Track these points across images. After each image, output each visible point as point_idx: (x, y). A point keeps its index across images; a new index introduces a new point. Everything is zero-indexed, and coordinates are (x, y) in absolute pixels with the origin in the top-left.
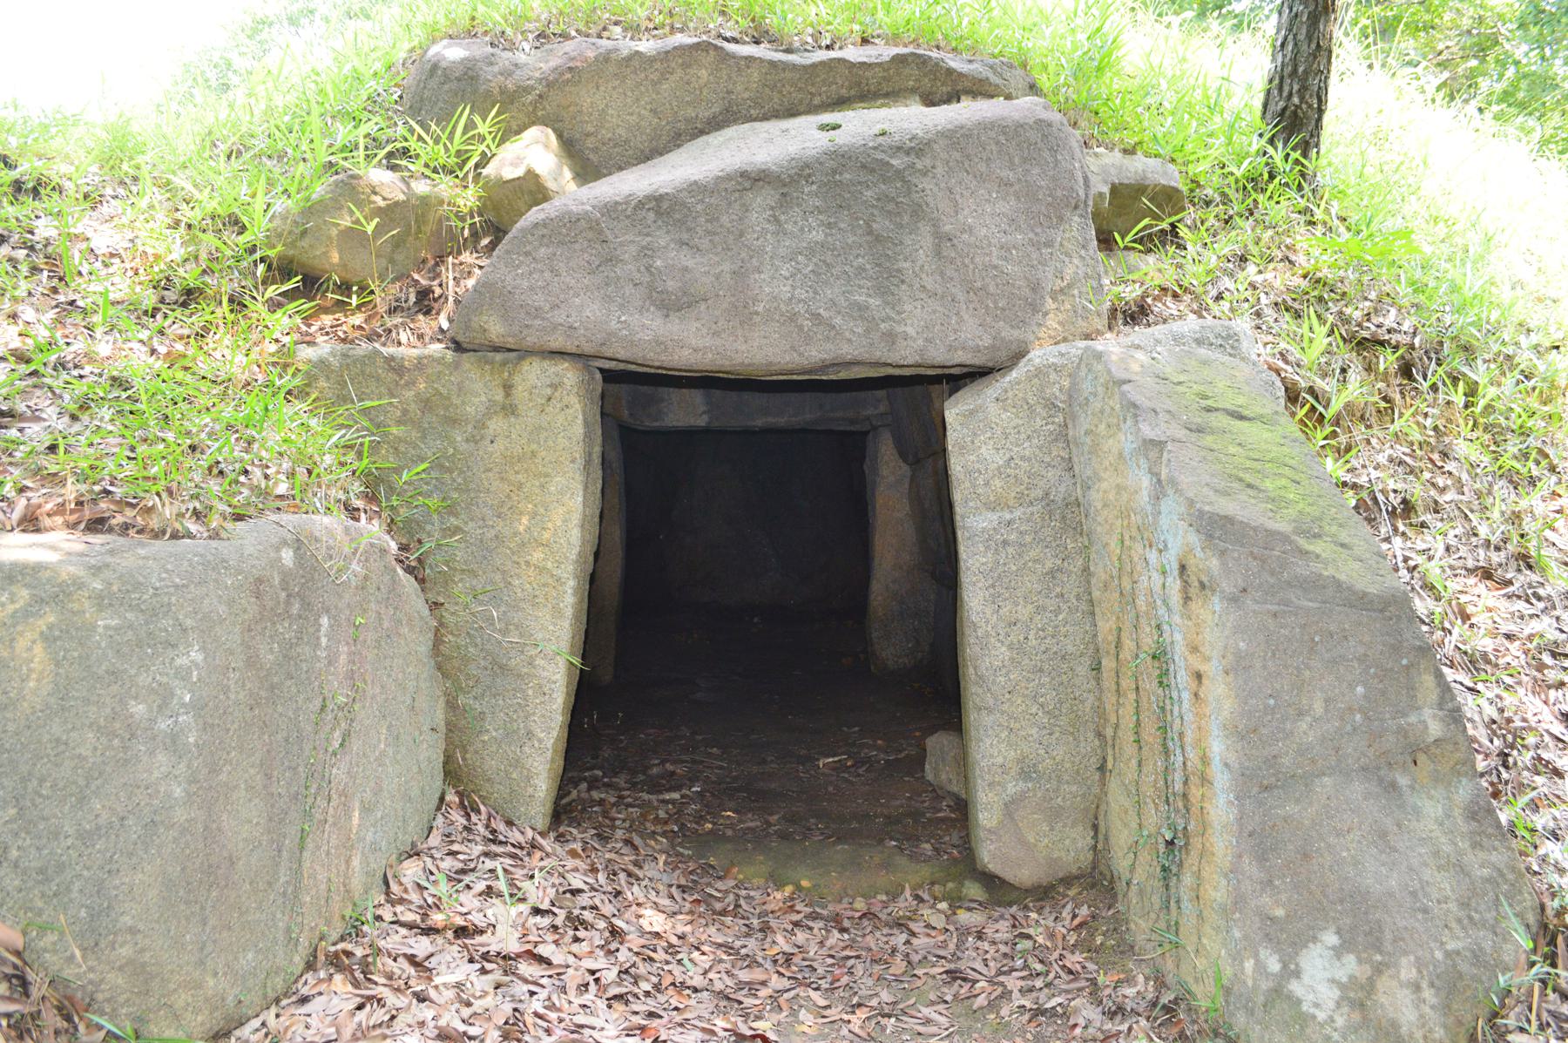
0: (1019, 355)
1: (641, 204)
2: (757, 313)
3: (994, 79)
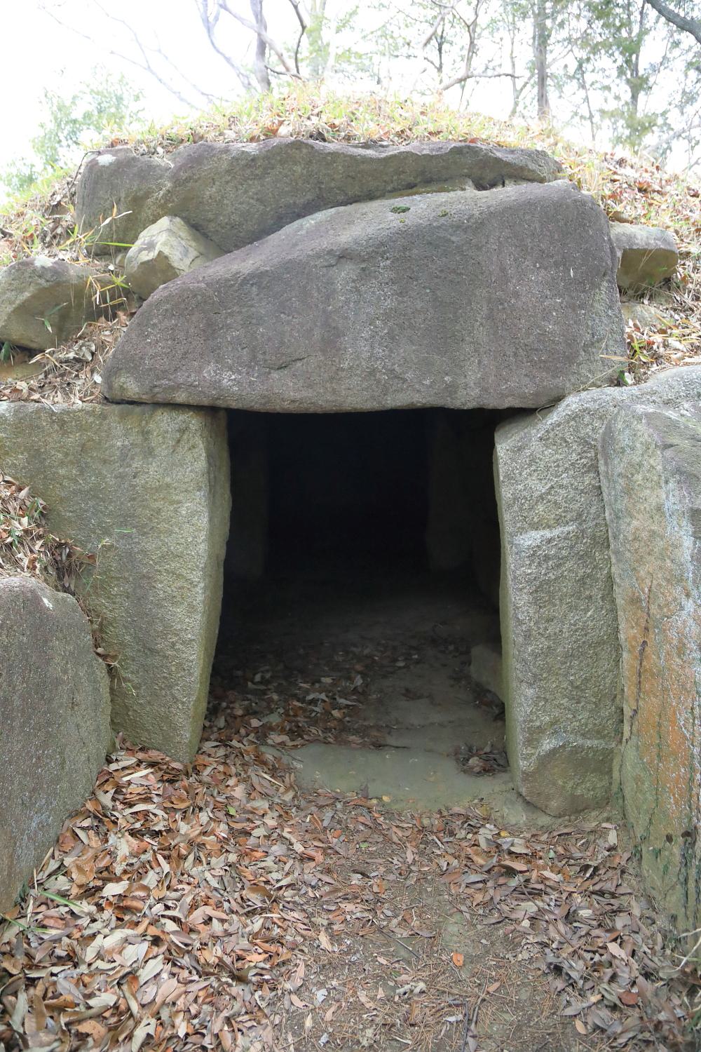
0: (558, 399)
1: (245, 281)
2: (343, 370)
3: (532, 166)
